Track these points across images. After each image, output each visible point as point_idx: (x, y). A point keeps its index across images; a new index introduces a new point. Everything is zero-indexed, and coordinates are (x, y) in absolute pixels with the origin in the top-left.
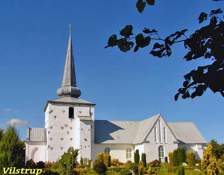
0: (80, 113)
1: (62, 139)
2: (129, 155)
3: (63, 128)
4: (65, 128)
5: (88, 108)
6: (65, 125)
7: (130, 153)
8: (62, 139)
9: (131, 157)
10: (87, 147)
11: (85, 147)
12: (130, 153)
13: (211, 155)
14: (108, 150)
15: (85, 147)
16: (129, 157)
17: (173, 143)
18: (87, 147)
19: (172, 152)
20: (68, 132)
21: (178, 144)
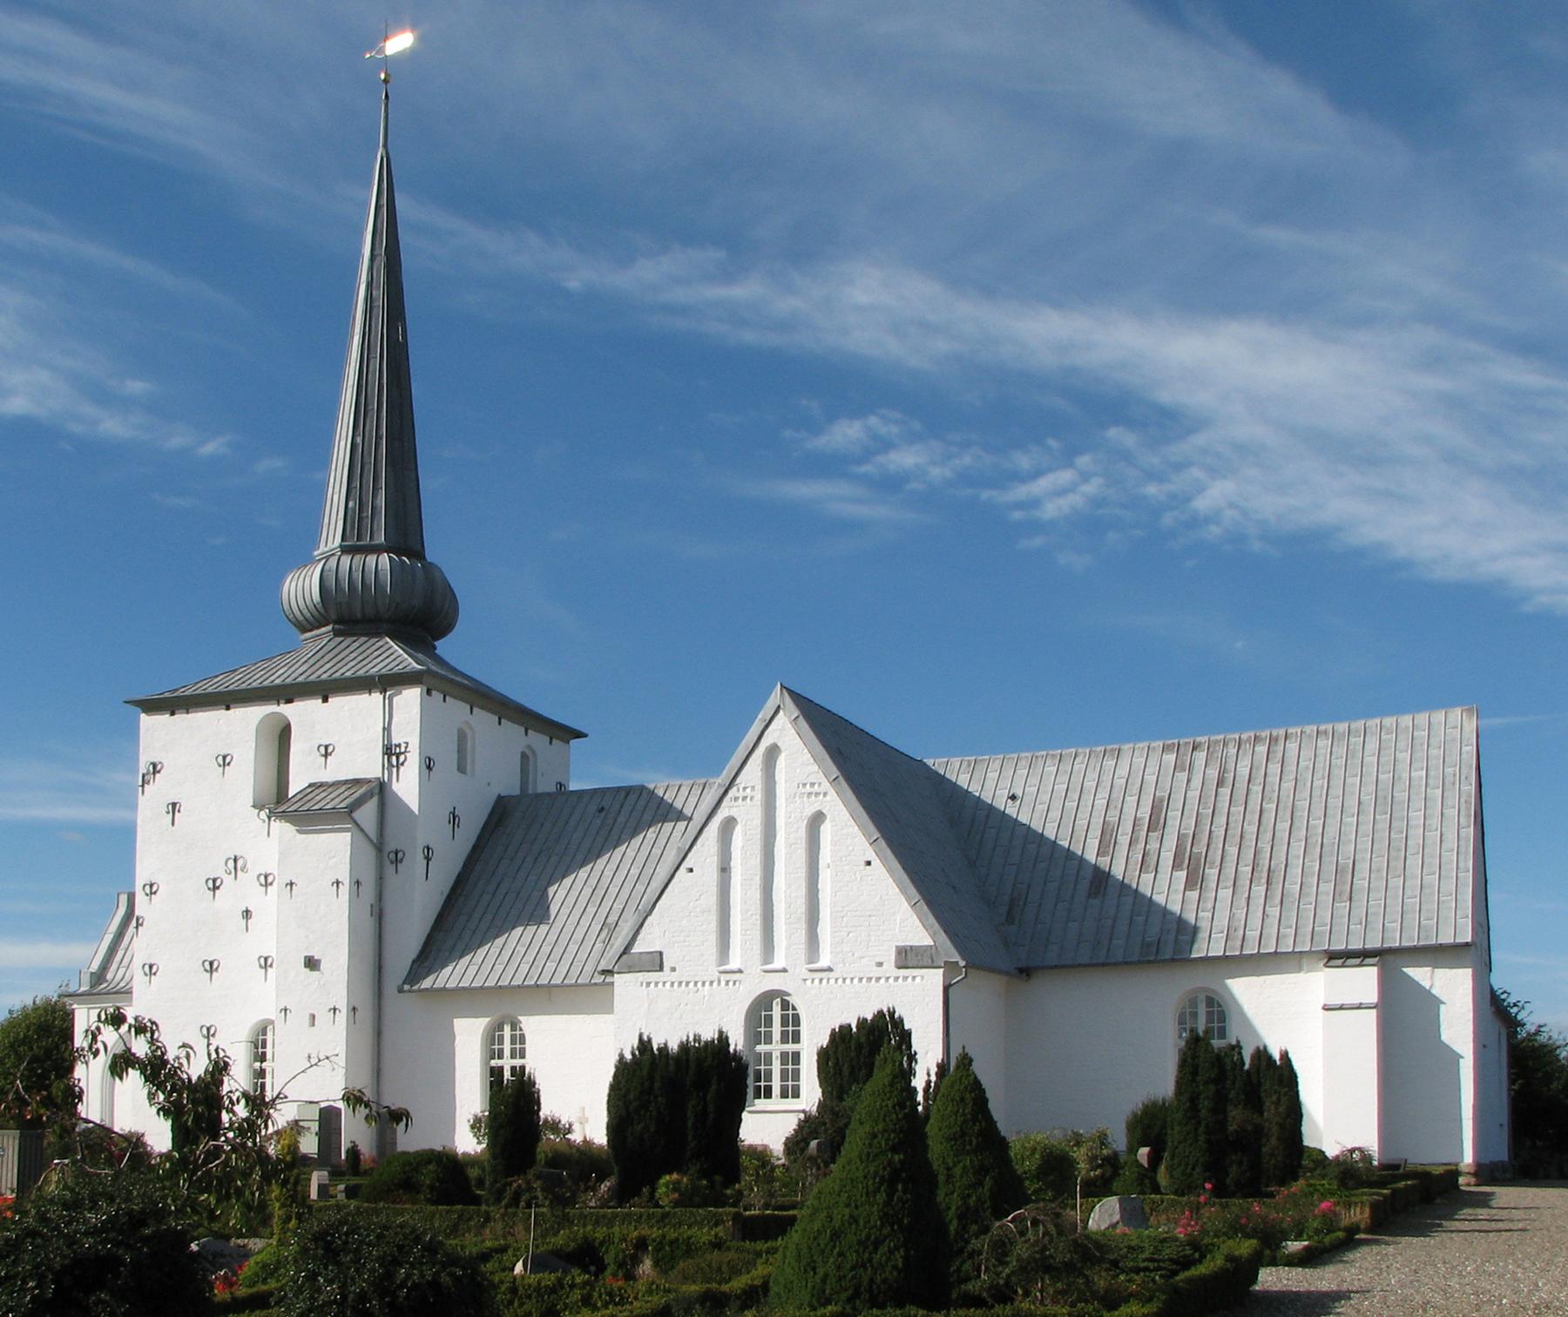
0: (326, 755)
1: (211, 967)
2: (776, 1067)
3: (215, 888)
4: (228, 880)
5: (372, 701)
6: (231, 864)
7: (790, 1047)
8: (211, 964)
9: (796, 1095)
10: (323, 1017)
11: (313, 1017)
12: (790, 1047)
13: (1477, 1300)
14: (513, 1041)
15: (313, 1017)
16: (776, 1090)
17: (890, 967)
18: (323, 1017)
19: (359, 1148)
20: (247, 914)
21: (950, 967)
